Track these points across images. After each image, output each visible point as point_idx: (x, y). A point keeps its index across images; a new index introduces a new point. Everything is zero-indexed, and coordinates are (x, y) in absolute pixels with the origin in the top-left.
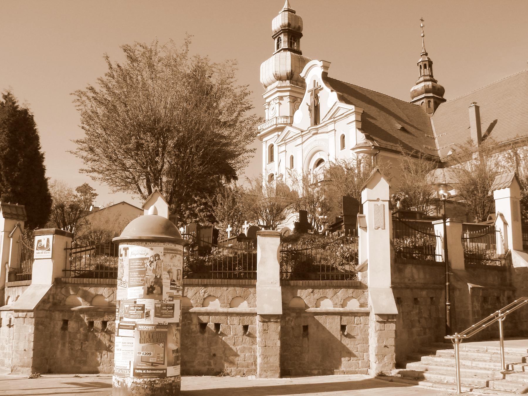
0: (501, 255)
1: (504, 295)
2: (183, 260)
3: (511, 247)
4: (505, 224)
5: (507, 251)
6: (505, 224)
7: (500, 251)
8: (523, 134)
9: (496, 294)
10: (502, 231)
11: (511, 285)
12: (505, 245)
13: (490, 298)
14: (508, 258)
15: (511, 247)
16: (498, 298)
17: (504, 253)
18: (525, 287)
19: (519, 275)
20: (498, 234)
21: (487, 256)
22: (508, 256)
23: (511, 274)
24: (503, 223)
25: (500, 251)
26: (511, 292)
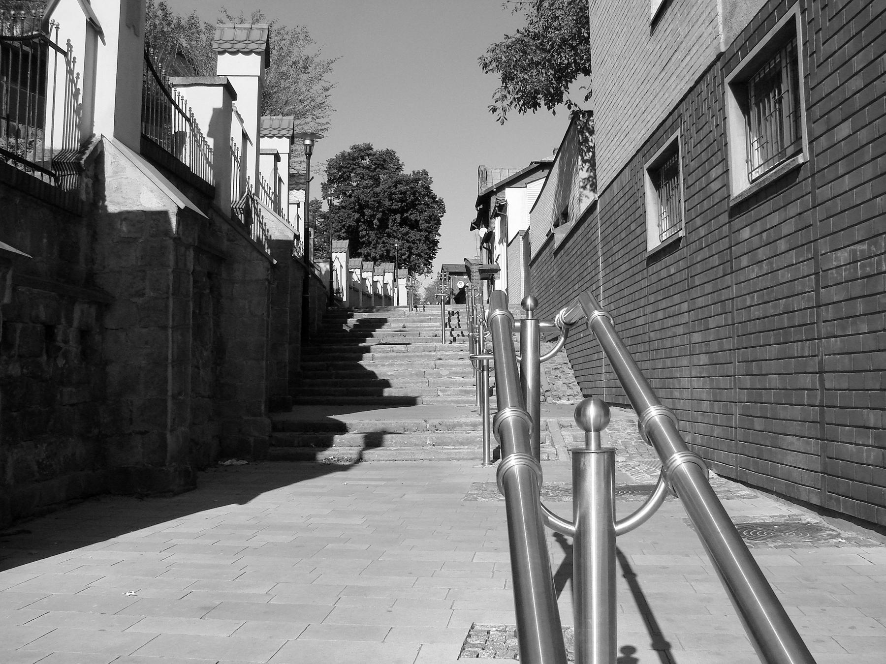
0: (63, 152)
1: (70, 322)
2: (551, 237)
3: (104, 125)
4: (94, 29)
5: (85, 142)
6: (94, 29)
7: (56, 136)
8: (884, 171)
9: (42, 313)
10: (79, 53)
11: (90, 279)
12: (82, 113)
13: (19, 326)
14: (91, 173)
15: (104, 125)
16: (49, 331)
17: (76, 145)
18: (149, 293)
19: (129, 241)
20: (56, 65)
21: (336, 202)
22: (88, 161)
23: (94, 237)
24: (83, 19)
25: (56, 136)
26: (93, 311)
